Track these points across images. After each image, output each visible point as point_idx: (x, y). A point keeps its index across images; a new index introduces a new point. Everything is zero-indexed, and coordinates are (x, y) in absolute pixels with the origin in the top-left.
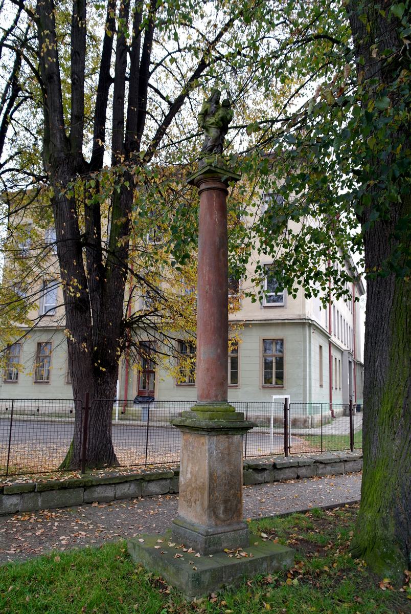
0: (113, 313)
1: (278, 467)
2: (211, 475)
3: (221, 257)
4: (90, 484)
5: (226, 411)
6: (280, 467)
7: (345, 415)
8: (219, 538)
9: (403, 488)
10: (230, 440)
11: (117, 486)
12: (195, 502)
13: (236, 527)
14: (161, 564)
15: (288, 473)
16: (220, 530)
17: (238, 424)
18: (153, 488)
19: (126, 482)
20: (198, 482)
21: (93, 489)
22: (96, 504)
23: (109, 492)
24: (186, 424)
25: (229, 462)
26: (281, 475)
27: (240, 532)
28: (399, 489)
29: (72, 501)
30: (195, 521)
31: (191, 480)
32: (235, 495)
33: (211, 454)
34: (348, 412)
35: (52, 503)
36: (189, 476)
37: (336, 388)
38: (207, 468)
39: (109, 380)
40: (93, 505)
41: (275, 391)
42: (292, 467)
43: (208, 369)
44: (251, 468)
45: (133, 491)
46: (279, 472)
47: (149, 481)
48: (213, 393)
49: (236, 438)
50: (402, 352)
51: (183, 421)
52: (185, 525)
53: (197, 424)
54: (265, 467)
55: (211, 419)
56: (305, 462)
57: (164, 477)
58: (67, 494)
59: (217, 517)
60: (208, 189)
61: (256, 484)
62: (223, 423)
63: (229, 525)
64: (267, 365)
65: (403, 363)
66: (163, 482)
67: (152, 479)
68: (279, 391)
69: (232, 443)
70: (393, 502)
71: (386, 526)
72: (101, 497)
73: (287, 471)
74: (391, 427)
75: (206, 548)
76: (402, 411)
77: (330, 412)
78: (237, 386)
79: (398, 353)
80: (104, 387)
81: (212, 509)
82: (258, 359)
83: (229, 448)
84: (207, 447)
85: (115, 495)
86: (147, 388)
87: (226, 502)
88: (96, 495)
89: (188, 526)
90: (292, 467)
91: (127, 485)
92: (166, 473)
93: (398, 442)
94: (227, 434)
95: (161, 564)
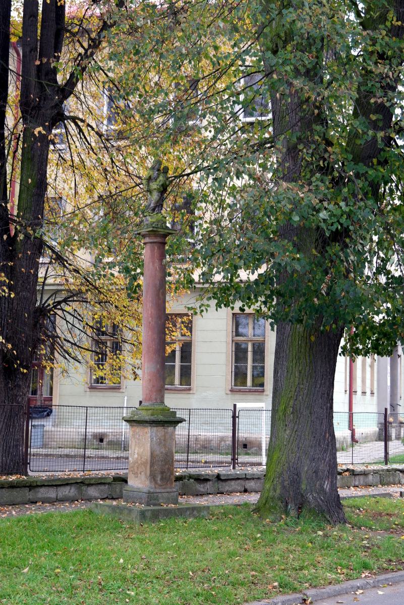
0: (25, 299)
1: (222, 478)
2: (152, 454)
3: (161, 296)
4: (35, 484)
5: (163, 410)
6: (225, 478)
7: (379, 439)
8: (157, 496)
9: (289, 464)
10: (166, 430)
11: (59, 488)
12: (141, 474)
13: (169, 490)
14: (118, 511)
15: (234, 485)
16: (158, 491)
17: (172, 419)
18: (92, 491)
19: (67, 484)
20: (143, 459)
21: (37, 489)
22: (41, 504)
23: (52, 493)
24: (134, 419)
25: (165, 445)
26: (226, 487)
27: (172, 494)
28: (286, 465)
29: (19, 500)
30: (140, 486)
31: (137, 459)
32: (169, 469)
33: (152, 439)
34: (383, 437)
35: (2, 500)
36: (136, 456)
37: (364, 393)
38: (149, 449)
39: (21, 383)
40: (38, 504)
41: (250, 396)
42: (238, 479)
43: (150, 380)
44: (192, 479)
45: (74, 494)
46: (224, 484)
47: (89, 485)
48: (153, 397)
49: (170, 429)
50: (294, 366)
51: (132, 417)
52: (133, 490)
53: (142, 419)
54: (207, 477)
55: (152, 415)
56: (254, 475)
57: (103, 481)
58: (15, 492)
59: (156, 483)
60: (151, 243)
61: (197, 495)
62: (161, 418)
63: (165, 488)
64: (239, 353)
65: (295, 374)
66: (102, 487)
67: (92, 483)
68: (258, 397)
69: (167, 433)
70: (282, 473)
71: (275, 490)
72: (44, 498)
73: (233, 483)
74: (284, 421)
75: (148, 501)
76: (291, 409)
77: (348, 433)
78: (190, 389)
79: (292, 367)
80: (15, 392)
81: (153, 477)
82: (225, 344)
83: (165, 436)
84: (149, 435)
85: (57, 497)
86: (39, 392)
87: (162, 473)
88: (40, 495)
89: (135, 490)
90: (238, 479)
91: (68, 488)
92: (105, 478)
93: (288, 432)
94: (163, 426)
95: (118, 511)
